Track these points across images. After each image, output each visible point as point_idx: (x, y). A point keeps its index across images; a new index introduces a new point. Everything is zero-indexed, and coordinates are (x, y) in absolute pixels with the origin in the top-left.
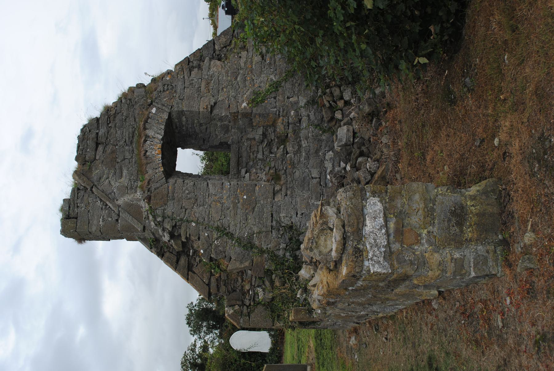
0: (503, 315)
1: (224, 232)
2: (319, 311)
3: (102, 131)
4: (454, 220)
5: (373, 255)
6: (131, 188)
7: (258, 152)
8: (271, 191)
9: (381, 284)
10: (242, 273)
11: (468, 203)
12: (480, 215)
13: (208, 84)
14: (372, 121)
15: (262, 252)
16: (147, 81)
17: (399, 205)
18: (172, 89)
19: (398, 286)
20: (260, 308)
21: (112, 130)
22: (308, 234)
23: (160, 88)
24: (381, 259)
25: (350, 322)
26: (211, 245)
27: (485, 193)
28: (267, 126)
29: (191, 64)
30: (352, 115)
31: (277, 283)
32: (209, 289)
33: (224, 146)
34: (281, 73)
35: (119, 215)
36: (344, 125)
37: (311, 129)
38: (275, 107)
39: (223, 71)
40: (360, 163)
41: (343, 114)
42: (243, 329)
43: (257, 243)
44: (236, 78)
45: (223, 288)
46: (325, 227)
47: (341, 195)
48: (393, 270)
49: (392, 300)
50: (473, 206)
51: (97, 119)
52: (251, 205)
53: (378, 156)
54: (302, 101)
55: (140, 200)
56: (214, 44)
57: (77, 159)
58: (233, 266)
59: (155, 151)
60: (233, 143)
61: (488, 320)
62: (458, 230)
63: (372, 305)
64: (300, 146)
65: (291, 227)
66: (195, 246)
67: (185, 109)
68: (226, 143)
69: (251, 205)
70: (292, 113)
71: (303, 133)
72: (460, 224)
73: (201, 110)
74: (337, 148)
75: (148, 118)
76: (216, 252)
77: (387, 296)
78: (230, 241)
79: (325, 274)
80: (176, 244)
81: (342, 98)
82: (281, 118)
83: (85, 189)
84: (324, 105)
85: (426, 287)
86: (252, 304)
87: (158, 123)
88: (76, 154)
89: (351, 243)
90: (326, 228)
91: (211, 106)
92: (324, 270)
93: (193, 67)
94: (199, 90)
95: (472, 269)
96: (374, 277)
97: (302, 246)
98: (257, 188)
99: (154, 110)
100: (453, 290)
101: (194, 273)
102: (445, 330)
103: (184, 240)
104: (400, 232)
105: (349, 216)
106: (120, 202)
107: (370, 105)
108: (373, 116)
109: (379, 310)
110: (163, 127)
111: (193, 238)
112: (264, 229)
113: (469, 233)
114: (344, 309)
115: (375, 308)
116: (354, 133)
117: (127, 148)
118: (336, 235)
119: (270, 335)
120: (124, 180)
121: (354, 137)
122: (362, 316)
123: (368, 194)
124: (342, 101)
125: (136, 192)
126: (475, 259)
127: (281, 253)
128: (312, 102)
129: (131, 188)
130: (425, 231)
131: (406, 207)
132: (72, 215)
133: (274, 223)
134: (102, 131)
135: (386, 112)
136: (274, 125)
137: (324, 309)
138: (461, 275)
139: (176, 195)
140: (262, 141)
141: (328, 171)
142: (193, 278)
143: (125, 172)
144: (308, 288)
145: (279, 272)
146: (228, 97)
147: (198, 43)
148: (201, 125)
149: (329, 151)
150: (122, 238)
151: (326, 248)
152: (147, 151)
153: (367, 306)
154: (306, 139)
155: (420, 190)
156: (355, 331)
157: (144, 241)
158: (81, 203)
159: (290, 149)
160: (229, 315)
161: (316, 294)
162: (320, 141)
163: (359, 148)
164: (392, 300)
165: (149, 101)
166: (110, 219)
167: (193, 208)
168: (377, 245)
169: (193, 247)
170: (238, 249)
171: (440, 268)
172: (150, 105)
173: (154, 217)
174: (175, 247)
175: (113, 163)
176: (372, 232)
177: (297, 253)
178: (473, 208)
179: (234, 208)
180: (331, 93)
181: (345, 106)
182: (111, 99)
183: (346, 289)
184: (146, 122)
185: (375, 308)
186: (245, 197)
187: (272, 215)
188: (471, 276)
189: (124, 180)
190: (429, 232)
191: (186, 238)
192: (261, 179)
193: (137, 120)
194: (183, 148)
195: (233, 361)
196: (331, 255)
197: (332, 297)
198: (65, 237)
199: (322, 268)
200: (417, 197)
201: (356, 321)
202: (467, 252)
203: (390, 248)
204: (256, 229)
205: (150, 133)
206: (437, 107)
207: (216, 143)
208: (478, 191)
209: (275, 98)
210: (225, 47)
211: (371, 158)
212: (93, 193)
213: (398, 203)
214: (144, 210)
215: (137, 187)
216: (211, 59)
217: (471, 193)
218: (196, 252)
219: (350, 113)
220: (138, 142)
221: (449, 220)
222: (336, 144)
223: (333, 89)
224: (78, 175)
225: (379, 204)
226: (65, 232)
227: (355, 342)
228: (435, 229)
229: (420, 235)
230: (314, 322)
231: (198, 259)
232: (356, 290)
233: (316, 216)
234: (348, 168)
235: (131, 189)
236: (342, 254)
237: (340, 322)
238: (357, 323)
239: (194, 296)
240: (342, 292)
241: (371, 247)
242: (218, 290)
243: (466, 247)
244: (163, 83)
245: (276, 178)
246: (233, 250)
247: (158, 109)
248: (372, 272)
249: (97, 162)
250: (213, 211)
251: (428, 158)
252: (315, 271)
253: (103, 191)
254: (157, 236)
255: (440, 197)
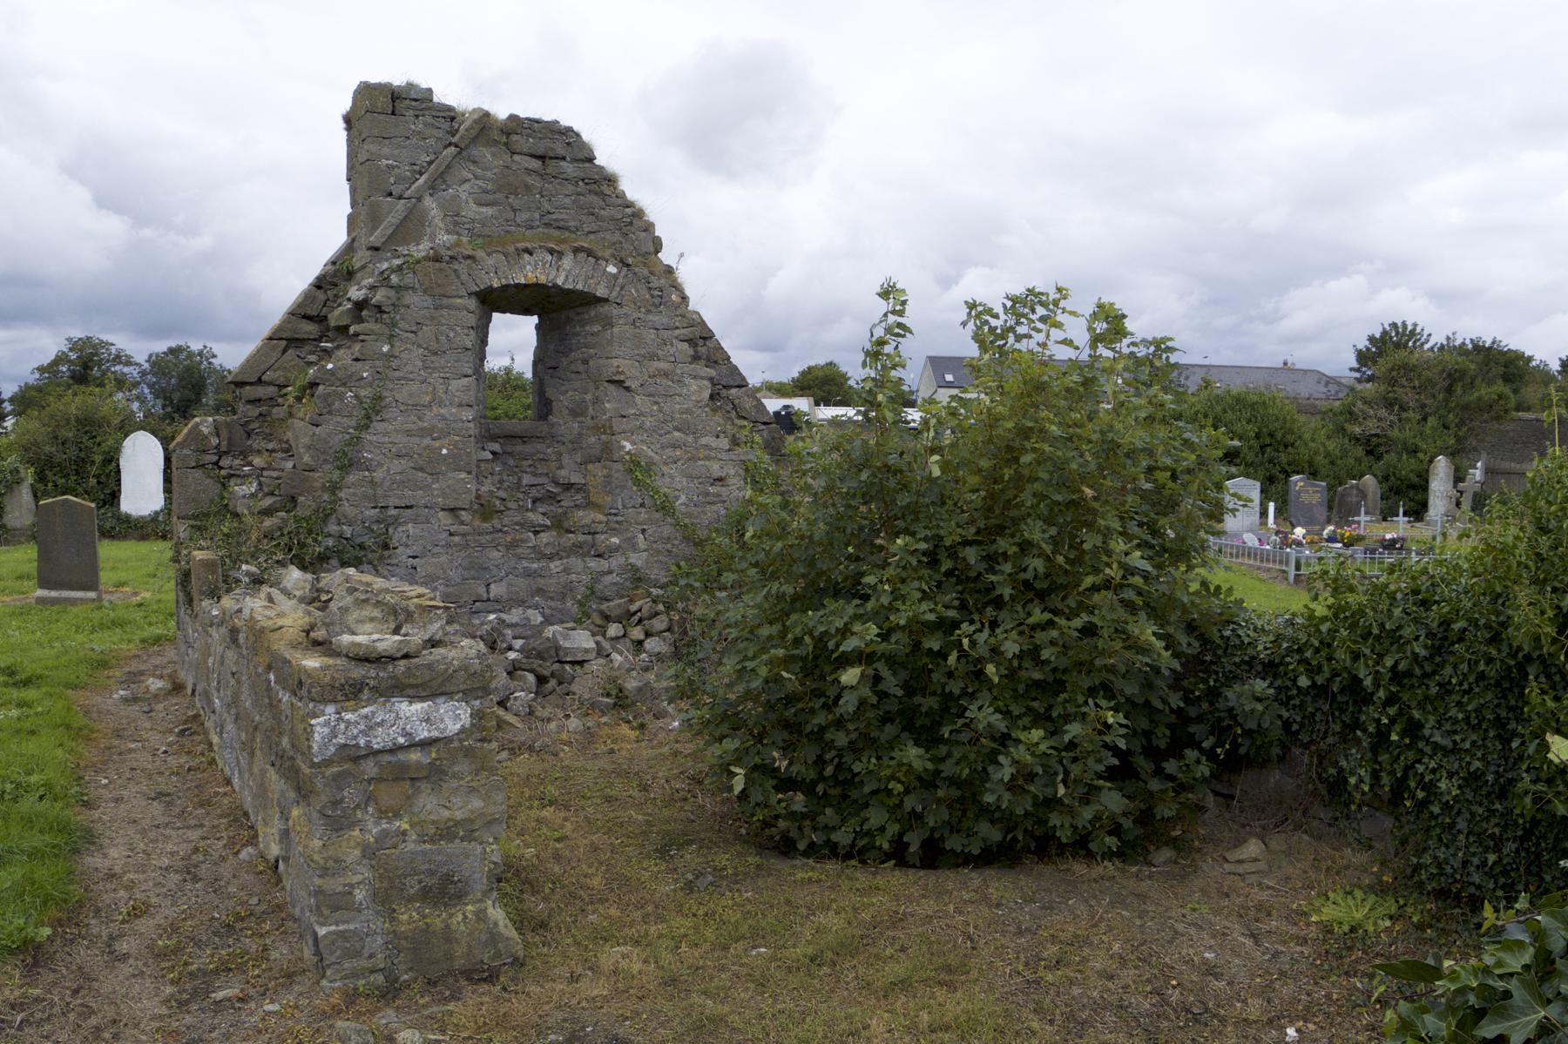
0: (241, 1000)
1: (373, 411)
2: (215, 613)
3: (568, 168)
4: (431, 881)
5: (348, 723)
6: (456, 224)
7: (535, 475)
8: (459, 504)
9: (285, 742)
10: (288, 451)
11: (470, 908)
12: (448, 935)
13: (666, 375)
14: (608, 695)
15: (334, 488)
16: (667, 257)
17: (456, 769)
18: (654, 304)
19: (283, 776)
20: (217, 488)
21: (571, 188)
22: (379, 583)
23: (655, 283)
24: (341, 740)
25: (196, 677)
26: (344, 384)
27: (494, 937)
28: (587, 492)
29: (701, 342)
30: (617, 657)
31: (268, 523)
32: (251, 384)
33: (544, 407)
34: (690, 515)
35: (400, 198)
36: (597, 643)
37: (585, 578)
38: (624, 506)
39: (690, 405)
40: (522, 678)
41: (617, 638)
42: (167, 460)
43: (351, 478)
44: (678, 429)
45: (254, 411)
46: (402, 617)
47: (468, 649)
48: (319, 765)
49: (250, 764)
50: (465, 917)
51: (591, 159)
52: (430, 466)
53: (540, 712)
54: (637, 559)
55: (433, 241)
56: (739, 386)
57: (513, 118)
58: (299, 431)
59: (531, 272)
60: (553, 425)
61: (224, 969)
62: (412, 891)
63: (236, 721)
64: (551, 558)
65: (386, 547)
66: (341, 352)
67: (616, 330)
68: (550, 412)
69: (430, 466)
70: (615, 540)
71: (575, 562)
72: (425, 895)
73: (615, 362)
74: (550, 631)
75: (597, 258)
76: (329, 395)
77: (258, 752)
78: (353, 423)
79: (300, 622)
80: (342, 313)
81: (648, 634)
82: (604, 519)
83: (453, 133)
84: (631, 601)
85: (285, 834)
86: (223, 472)
87: (587, 278)
88: (523, 115)
89: (373, 673)
90: (398, 617)
91: (621, 382)
92: (307, 619)
93: (696, 345)
94: (653, 357)
95: (333, 928)
96: (301, 726)
97: (351, 571)
98: (463, 475)
99: (612, 269)
100: (283, 888)
101: (284, 351)
102: (196, 879)
103: (352, 330)
104: (401, 774)
105: (430, 666)
106: (428, 202)
107: (640, 690)
108: (621, 701)
109: (224, 737)
110: (580, 287)
111: (357, 347)
112: (380, 492)
113: (408, 917)
114: (222, 663)
115: (230, 727)
116: (581, 663)
117: (537, 216)
118: (388, 642)
119: (156, 513)
120: (472, 210)
121: (573, 663)
122: (210, 702)
123: (477, 703)
124: (642, 637)
125: (448, 232)
126: (354, 932)
127: (332, 528)
128: (638, 579)
129: (456, 224)
130: (406, 826)
131: (455, 783)
132: (400, 105)
133: (393, 512)
134: (568, 168)
135: (628, 722)
136: (589, 505)
137: (222, 623)
138: (318, 907)
139: (444, 312)
140: (557, 484)
141: (503, 616)
142: (273, 348)
143: (488, 211)
144: (265, 589)
145: (291, 526)
146: (641, 414)
147: (739, 358)
148: (585, 362)
149: (543, 614)
150: (354, 204)
151: (358, 621)
152: (531, 254)
153: (233, 711)
154: (564, 570)
155: (492, 809)
156: (177, 688)
157: (349, 249)
158: (425, 124)
159: (545, 537)
160: (197, 425)
161: (255, 605)
162: (563, 597)
163: (553, 675)
164: (250, 764)
165: (630, 260)
166: (392, 180)
167: (419, 346)
168: (370, 728)
169: (338, 347)
170: (337, 441)
171: (331, 863)
172: (622, 261)
173: (400, 268)
174: (337, 312)
175: (506, 189)
176: (398, 717)
177: (334, 562)
178: (460, 917)
179: (422, 429)
180: (657, 614)
181: (633, 641)
182: (631, 189)
183: (269, 668)
184: (589, 253)
185: (230, 727)
186: (444, 451)
187: (411, 507)
188: (317, 928)
189: (472, 210)
190: (404, 833)
191: (357, 335)
192: (482, 484)
193: (592, 237)
194: (538, 327)
195: (98, 439)
196: (343, 632)
197: (249, 639)
198: (568, 136)
199: (309, 613)
200: (476, 803)
201: (199, 688)
202: (368, 914)
203: (366, 756)
204: (378, 475)
205: (567, 262)
206: (648, 822)
207: (550, 393)
208: (496, 924)
209: (642, 505)
210: (735, 408)
211: (534, 700)
212: (446, 147)
213: (463, 767)
214: (413, 248)
215: (458, 234)
216: (711, 379)
217: (490, 911)
218: (328, 353)
219: (621, 653)
220: (549, 238)
221: (431, 873)
222: (556, 627)
223: (664, 617)
224: (481, 118)
225: (458, 726)
226: (366, 92)
227: (153, 688)
228: (411, 846)
229: (397, 815)
230: (190, 601)
231: (313, 358)
232: (269, 689)
233: (419, 596)
234: (512, 655)
235: (455, 221)
236: (347, 656)
237: (194, 656)
238: (194, 691)
239: (231, 356)
240: (264, 659)
241: (366, 717)
242: (249, 402)
243: (377, 912)
244: (663, 288)
245: (485, 510)
246: (335, 430)
247: (615, 277)
248: (313, 722)
249: (507, 157)
250: (414, 387)
251: (547, 813)
252: (302, 600)
253: (448, 167)
254: (359, 275)
255: (479, 849)
